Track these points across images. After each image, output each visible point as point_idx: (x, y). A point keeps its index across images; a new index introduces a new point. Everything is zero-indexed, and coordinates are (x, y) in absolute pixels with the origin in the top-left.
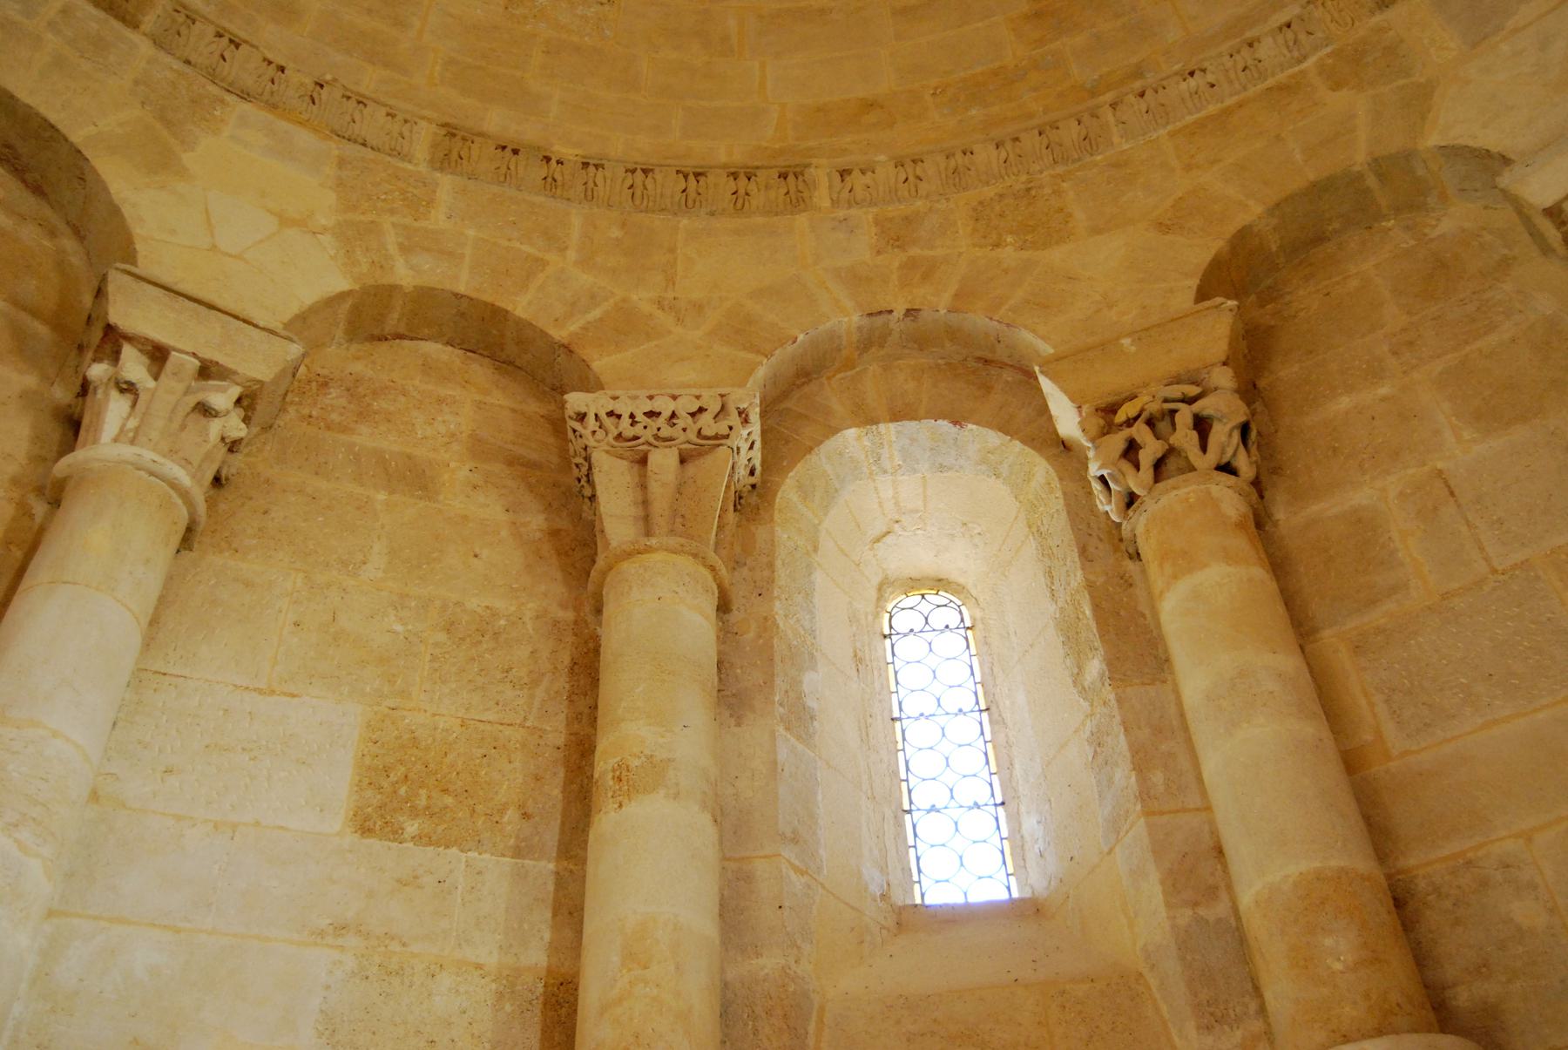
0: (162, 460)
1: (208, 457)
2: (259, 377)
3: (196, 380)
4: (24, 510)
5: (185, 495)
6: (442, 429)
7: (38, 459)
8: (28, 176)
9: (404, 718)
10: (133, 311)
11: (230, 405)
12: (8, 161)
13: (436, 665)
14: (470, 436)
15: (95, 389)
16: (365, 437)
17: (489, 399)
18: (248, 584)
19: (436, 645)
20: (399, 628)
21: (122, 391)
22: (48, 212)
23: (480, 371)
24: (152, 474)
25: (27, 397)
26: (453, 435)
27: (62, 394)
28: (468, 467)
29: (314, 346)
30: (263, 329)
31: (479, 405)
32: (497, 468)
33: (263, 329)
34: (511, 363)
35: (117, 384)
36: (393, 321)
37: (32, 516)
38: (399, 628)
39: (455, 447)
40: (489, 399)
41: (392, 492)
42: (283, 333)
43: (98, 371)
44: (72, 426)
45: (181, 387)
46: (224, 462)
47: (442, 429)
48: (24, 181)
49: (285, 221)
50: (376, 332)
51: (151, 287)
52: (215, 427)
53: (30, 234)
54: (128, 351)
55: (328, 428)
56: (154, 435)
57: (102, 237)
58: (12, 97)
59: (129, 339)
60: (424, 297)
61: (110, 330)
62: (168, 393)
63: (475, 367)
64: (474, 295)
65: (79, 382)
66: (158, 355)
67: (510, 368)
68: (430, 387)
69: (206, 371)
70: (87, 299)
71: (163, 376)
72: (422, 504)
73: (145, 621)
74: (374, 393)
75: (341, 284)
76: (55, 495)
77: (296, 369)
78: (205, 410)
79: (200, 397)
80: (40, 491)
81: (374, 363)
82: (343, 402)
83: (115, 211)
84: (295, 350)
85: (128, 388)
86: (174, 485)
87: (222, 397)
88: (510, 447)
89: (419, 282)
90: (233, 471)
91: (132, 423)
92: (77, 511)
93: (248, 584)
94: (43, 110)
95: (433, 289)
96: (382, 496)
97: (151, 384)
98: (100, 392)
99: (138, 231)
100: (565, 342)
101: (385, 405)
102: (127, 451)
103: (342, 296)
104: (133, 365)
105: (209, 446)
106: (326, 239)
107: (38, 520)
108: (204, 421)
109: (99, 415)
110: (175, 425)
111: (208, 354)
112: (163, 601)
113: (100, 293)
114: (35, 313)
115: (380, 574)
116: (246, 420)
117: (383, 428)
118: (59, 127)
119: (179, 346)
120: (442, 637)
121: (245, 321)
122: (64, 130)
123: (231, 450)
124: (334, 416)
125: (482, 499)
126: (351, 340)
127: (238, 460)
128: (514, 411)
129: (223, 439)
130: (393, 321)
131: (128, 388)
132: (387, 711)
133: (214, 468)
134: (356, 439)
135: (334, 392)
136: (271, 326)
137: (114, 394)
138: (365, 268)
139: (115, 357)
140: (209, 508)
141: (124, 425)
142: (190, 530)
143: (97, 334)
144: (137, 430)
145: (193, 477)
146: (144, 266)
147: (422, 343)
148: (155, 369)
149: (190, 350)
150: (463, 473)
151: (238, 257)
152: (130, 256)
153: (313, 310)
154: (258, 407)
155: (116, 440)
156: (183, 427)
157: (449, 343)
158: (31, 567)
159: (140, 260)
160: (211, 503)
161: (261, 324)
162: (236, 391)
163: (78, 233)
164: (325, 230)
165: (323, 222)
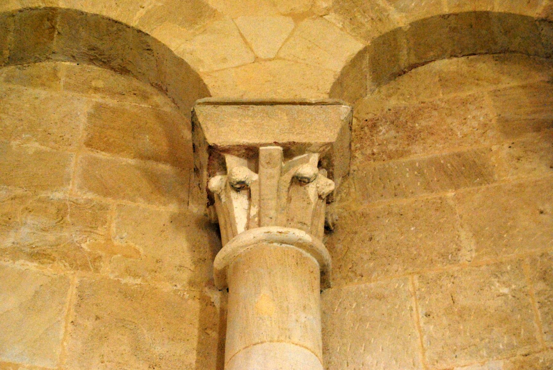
0: (284, 230)
1: (315, 214)
2: (327, 140)
3: (284, 161)
4: (206, 302)
5: (310, 248)
6: (475, 124)
7: (199, 262)
8: (112, 64)
9: (538, 359)
10: (223, 130)
11: (316, 170)
12: (97, 59)
13: (546, 309)
14: (499, 121)
15: (219, 197)
16: (419, 154)
17: (501, 86)
18: (381, 297)
19: (539, 293)
20: (505, 290)
21: (238, 190)
22: (135, 83)
23: (485, 67)
24: (282, 242)
25: (174, 219)
26: (485, 125)
27: (197, 209)
28: (506, 146)
29: (354, 100)
30: (316, 104)
31: (496, 94)
32: (529, 137)
33: (316, 104)
34: (505, 51)
35: (232, 186)
36: (405, 58)
37: (212, 304)
38: (505, 290)
39: (490, 133)
40: (501, 86)
41: (457, 187)
42: (331, 101)
43: (216, 182)
44: (213, 229)
45: (275, 171)
46: (327, 213)
47: (475, 124)
48: (112, 68)
49: (297, 17)
50: (396, 70)
51: (228, 107)
52: (312, 190)
53: (130, 104)
54: (231, 160)
55: (390, 158)
56: (272, 213)
57: (181, 86)
58: (82, 13)
59: (228, 150)
60: (421, 28)
61: (212, 149)
62: (269, 178)
63: (481, 66)
64: (456, 10)
65: (205, 195)
66: (251, 154)
67: (507, 55)
68: (452, 95)
69: (289, 151)
70: (187, 134)
71: (261, 168)
72: (483, 187)
73: (320, 353)
74: (413, 117)
75: (357, 46)
76: (222, 283)
77: (351, 123)
78: (300, 181)
79: (292, 172)
80: (210, 283)
81: (403, 94)
82: (393, 133)
83: (180, 63)
84: (345, 109)
85: (241, 187)
86: (300, 244)
87: (308, 167)
88: (533, 116)
89: (411, 19)
90: (335, 217)
91: (254, 211)
92: (242, 289)
93: (381, 297)
94: (104, 14)
95: (425, 20)
96: (450, 194)
97: (255, 177)
98: (223, 197)
99: (201, 70)
100: (544, 16)
101: (424, 123)
102: (259, 233)
103: (361, 54)
104: (238, 169)
105: (313, 206)
106: (332, 17)
107: (218, 305)
108: (302, 188)
109: (229, 214)
110: (284, 200)
111: (285, 139)
112: (324, 332)
113: (195, 126)
114: (157, 159)
115: (474, 254)
116: (330, 176)
117: (430, 141)
118: (120, 20)
119: (263, 141)
120: (541, 286)
121: (301, 104)
122: (124, 21)
123: (328, 203)
124: (391, 147)
125: (528, 166)
126: (379, 85)
127: (335, 207)
128: (523, 87)
129: (320, 197)
130: (405, 57)
131: (241, 187)
132: (522, 358)
133: (323, 220)
134: (413, 157)
135: (383, 129)
136: (320, 100)
137: (233, 194)
138: (368, 26)
139: (223, 168)
140: (330, 251)
141: (249, 214)
142: (323, 273)
143: (204, 156)
144: (259, 214)
145: (311, 233)
146: (218, 93)
147: (432, 64)
148: (224, 172)
149: (271, 141)
150: (505, 151)
151: (277, 58)
152: (204, 91)
153: (345, 73)
154: (335, 163)
155: (248, 227)
156: (289, 200)
157: (453, 55)
158: (228, 341)
159: (211, 92)
160: (330, 247)
161: (313, 100)
162: (315, 158)
163: (162, 89)
164: (328, 10)
165: (325, 5)
